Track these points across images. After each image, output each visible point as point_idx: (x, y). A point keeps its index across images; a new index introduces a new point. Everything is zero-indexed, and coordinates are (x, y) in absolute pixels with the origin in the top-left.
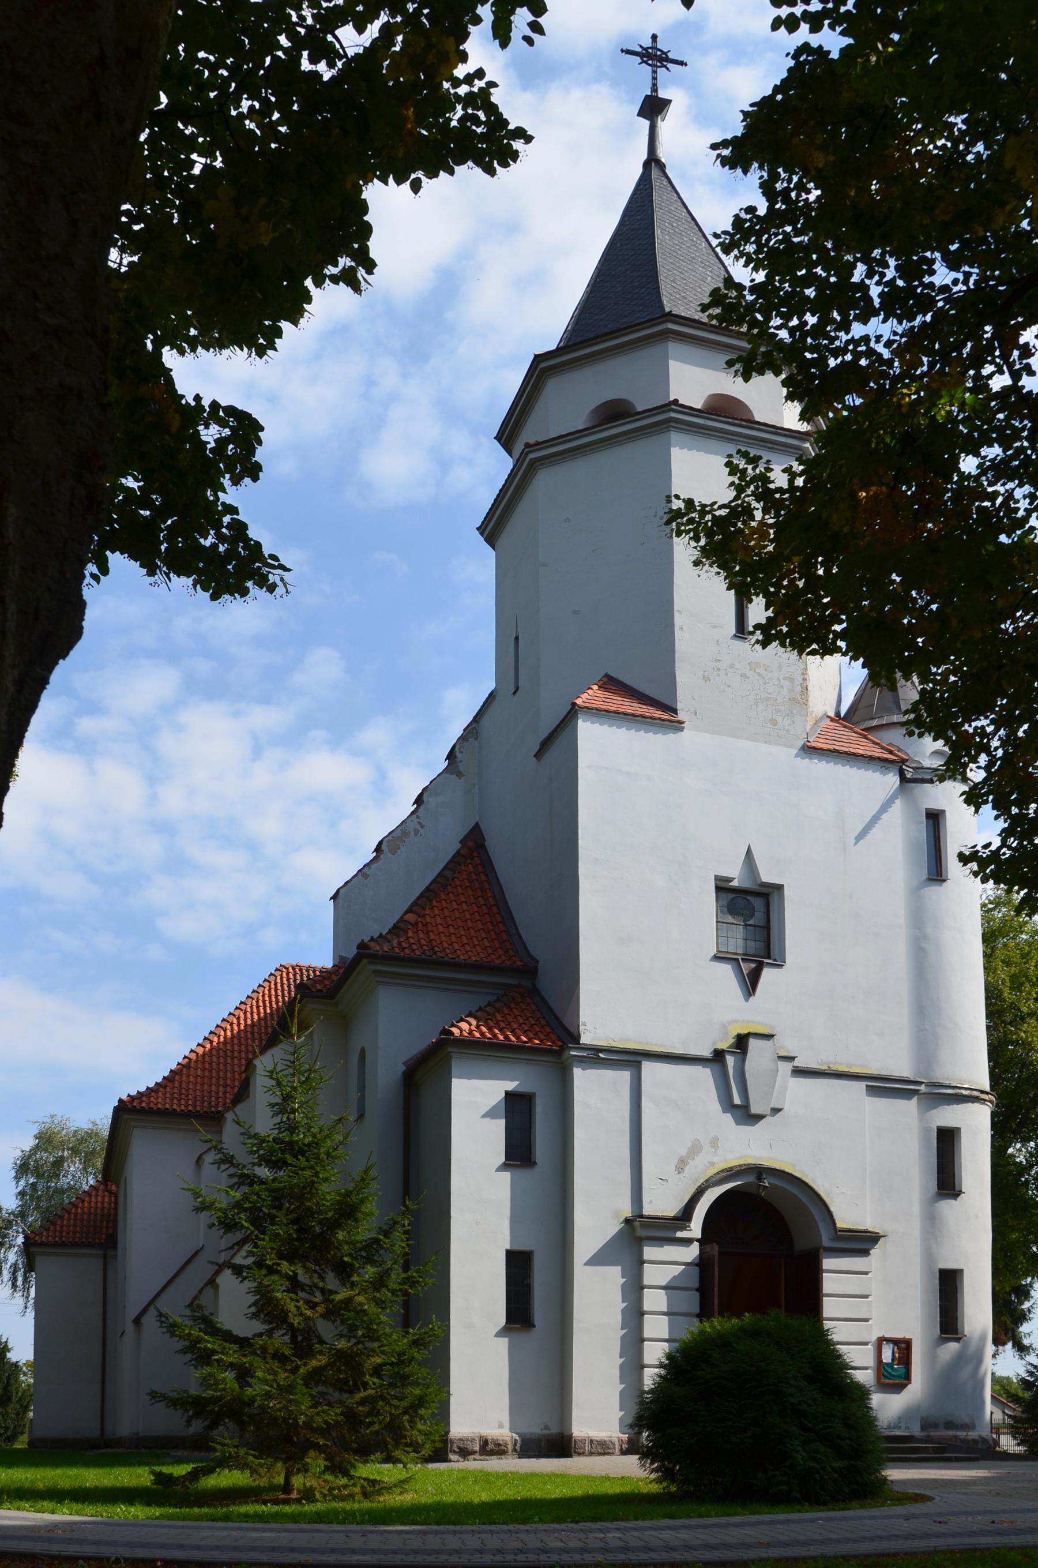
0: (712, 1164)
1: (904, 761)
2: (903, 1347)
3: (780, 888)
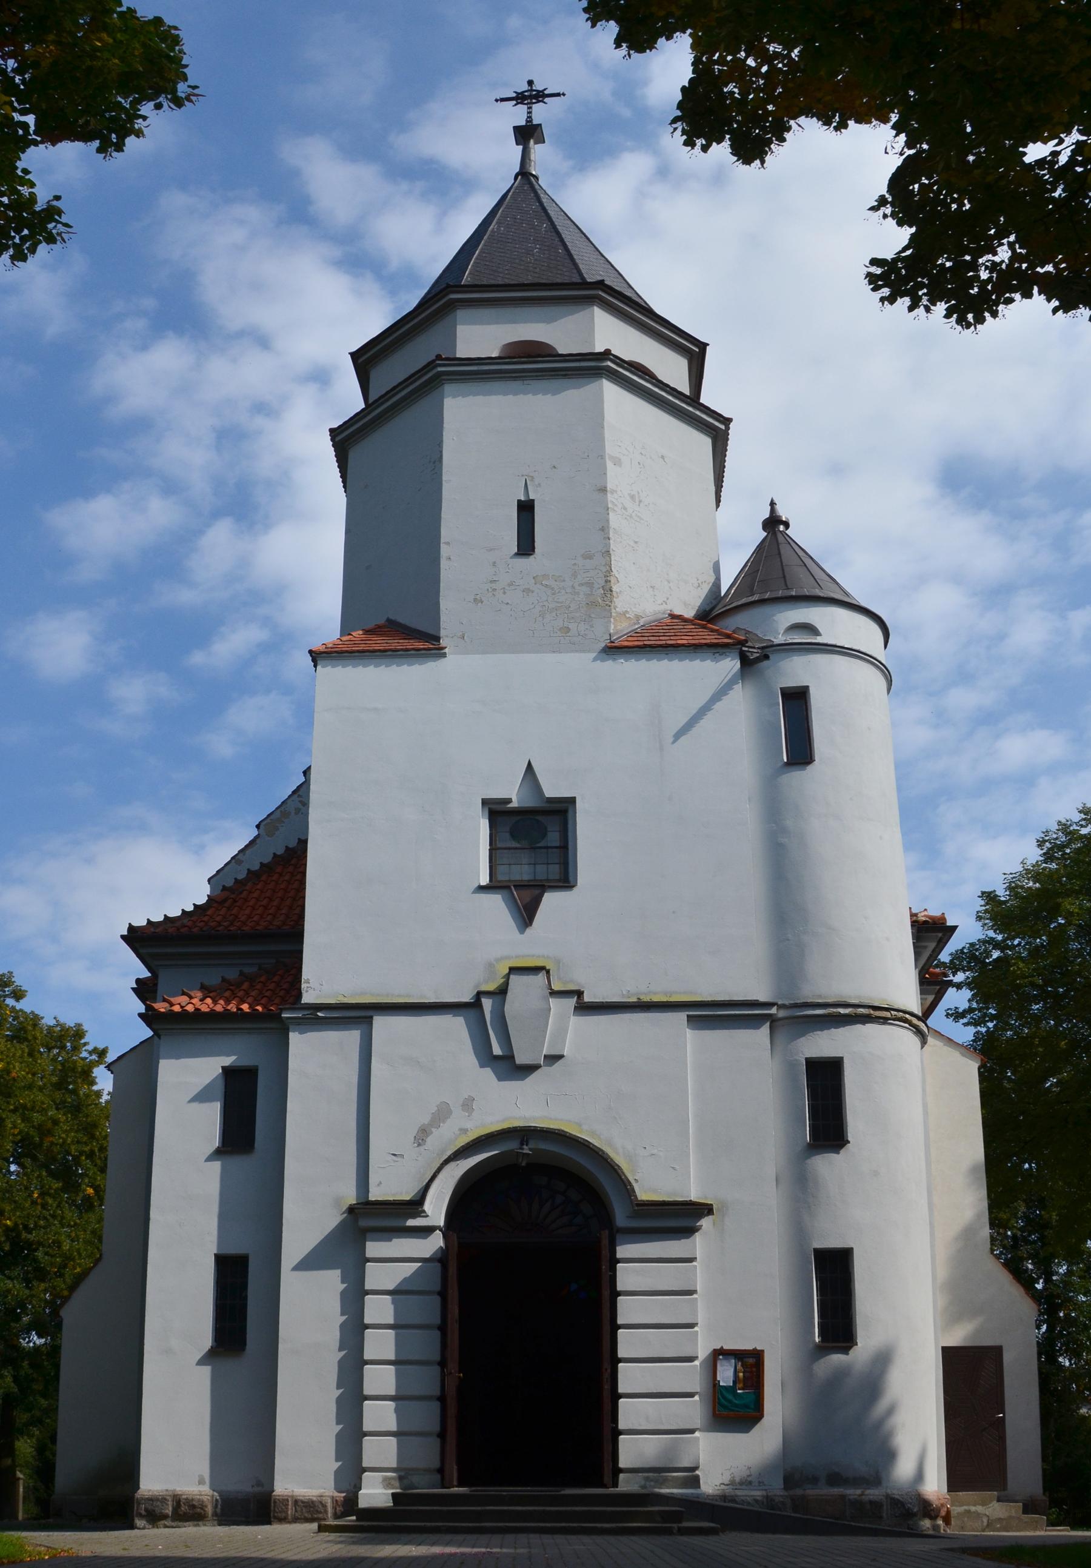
0: (464, 1131)
1: (743, 643)
2: (751, 1363)
3: (572, 801)
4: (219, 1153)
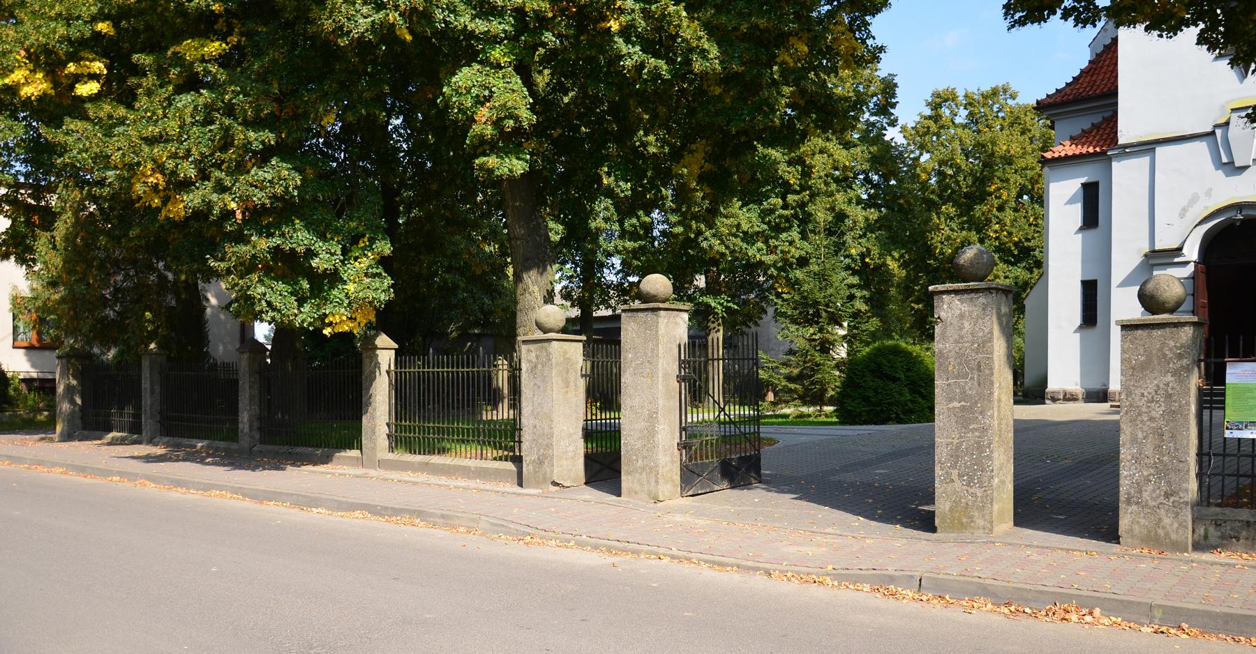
4: (1081, 229)
